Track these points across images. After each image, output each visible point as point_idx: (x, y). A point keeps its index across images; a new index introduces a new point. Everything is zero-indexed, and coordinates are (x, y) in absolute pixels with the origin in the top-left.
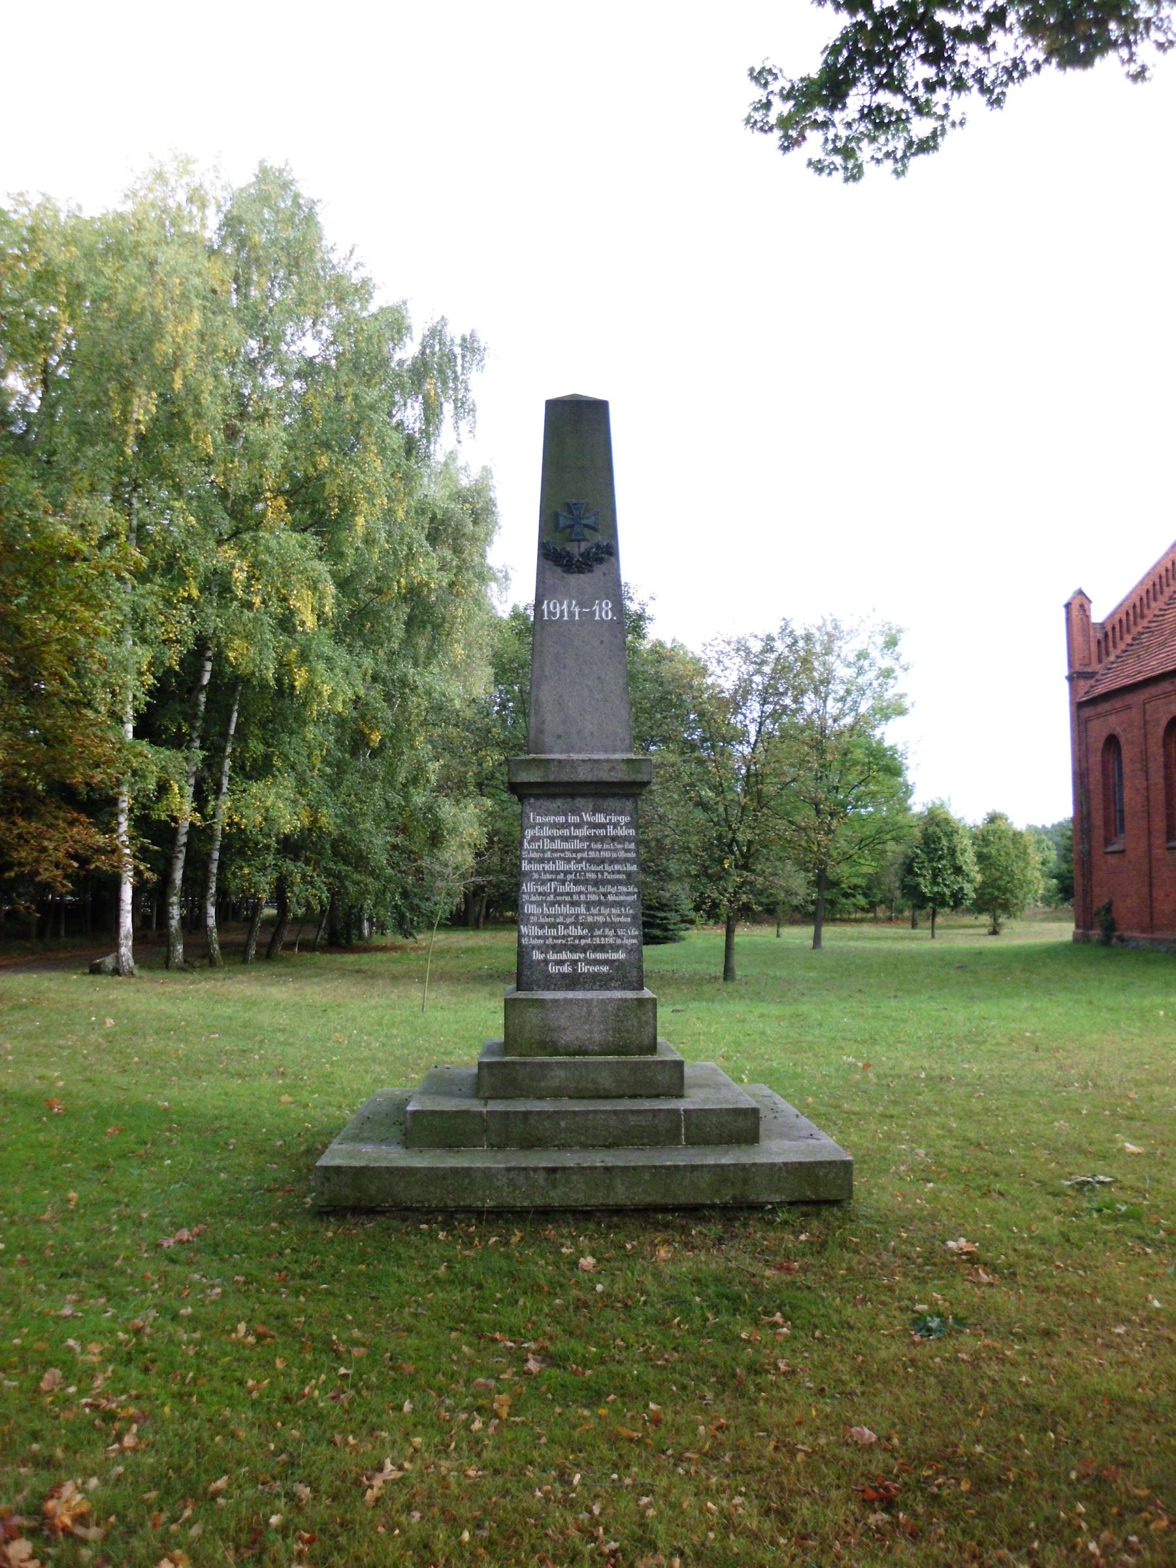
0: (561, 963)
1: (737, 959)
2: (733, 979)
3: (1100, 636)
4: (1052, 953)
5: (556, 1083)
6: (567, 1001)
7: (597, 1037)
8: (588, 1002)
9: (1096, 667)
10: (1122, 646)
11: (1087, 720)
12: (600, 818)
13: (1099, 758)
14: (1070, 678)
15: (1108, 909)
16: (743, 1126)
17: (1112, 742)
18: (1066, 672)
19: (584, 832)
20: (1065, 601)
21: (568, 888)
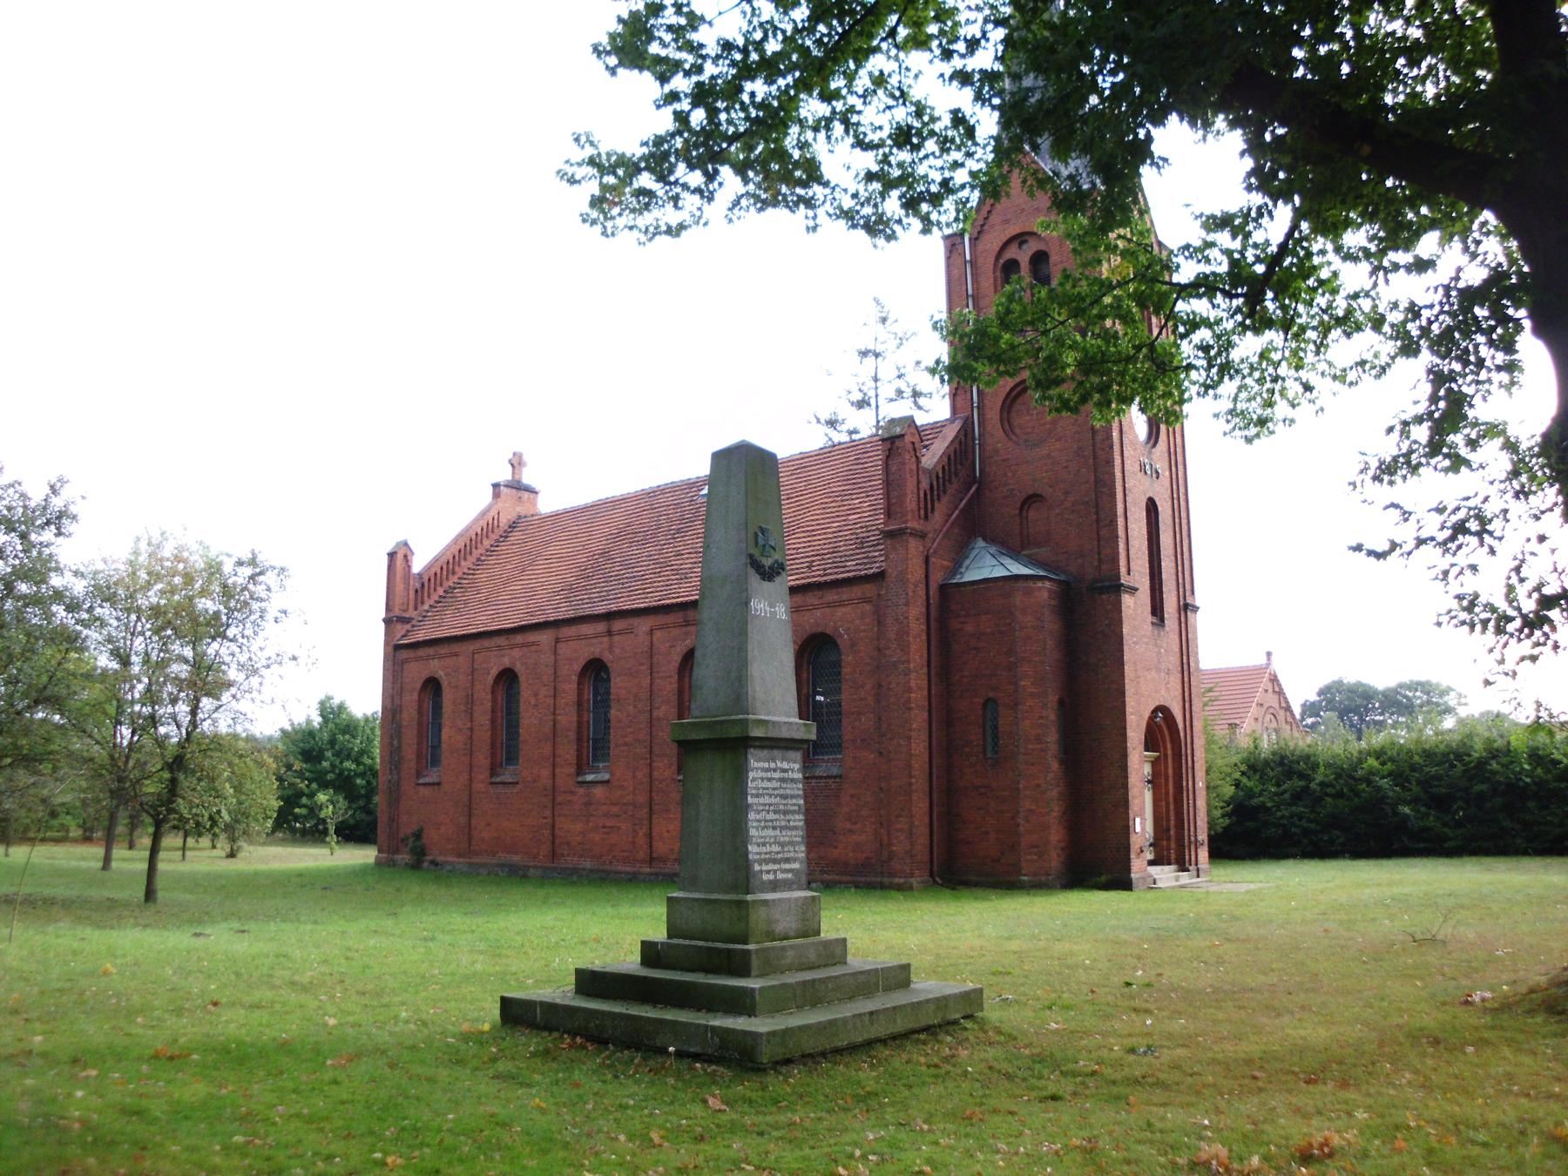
0: (768, 872)
1: (160, 883)
2: (155, 901)
3: (418, 585)
4: (360, 873)
5: (789, 961)
6: (780, 900)
7: (794, 926)
8: (789, 900)
9: (411, 613)
10: (435, 597)
11: (404, 662)
12: (785, 765)
13: (415, 695)
14: (384, 620)
15: (418, 835)
16: (899, 977)
17: (432, 686)
18: (383, 615)
19: (777, 775)
20: (389, 548)
21: (772, 816)
